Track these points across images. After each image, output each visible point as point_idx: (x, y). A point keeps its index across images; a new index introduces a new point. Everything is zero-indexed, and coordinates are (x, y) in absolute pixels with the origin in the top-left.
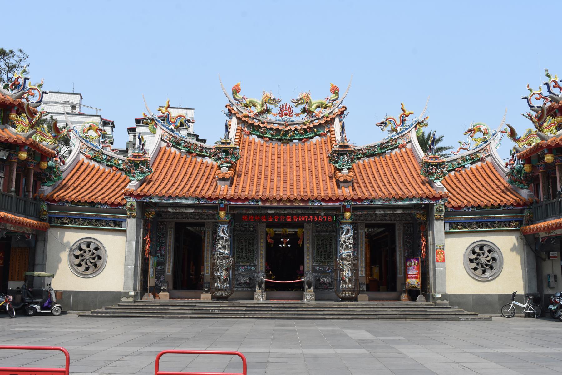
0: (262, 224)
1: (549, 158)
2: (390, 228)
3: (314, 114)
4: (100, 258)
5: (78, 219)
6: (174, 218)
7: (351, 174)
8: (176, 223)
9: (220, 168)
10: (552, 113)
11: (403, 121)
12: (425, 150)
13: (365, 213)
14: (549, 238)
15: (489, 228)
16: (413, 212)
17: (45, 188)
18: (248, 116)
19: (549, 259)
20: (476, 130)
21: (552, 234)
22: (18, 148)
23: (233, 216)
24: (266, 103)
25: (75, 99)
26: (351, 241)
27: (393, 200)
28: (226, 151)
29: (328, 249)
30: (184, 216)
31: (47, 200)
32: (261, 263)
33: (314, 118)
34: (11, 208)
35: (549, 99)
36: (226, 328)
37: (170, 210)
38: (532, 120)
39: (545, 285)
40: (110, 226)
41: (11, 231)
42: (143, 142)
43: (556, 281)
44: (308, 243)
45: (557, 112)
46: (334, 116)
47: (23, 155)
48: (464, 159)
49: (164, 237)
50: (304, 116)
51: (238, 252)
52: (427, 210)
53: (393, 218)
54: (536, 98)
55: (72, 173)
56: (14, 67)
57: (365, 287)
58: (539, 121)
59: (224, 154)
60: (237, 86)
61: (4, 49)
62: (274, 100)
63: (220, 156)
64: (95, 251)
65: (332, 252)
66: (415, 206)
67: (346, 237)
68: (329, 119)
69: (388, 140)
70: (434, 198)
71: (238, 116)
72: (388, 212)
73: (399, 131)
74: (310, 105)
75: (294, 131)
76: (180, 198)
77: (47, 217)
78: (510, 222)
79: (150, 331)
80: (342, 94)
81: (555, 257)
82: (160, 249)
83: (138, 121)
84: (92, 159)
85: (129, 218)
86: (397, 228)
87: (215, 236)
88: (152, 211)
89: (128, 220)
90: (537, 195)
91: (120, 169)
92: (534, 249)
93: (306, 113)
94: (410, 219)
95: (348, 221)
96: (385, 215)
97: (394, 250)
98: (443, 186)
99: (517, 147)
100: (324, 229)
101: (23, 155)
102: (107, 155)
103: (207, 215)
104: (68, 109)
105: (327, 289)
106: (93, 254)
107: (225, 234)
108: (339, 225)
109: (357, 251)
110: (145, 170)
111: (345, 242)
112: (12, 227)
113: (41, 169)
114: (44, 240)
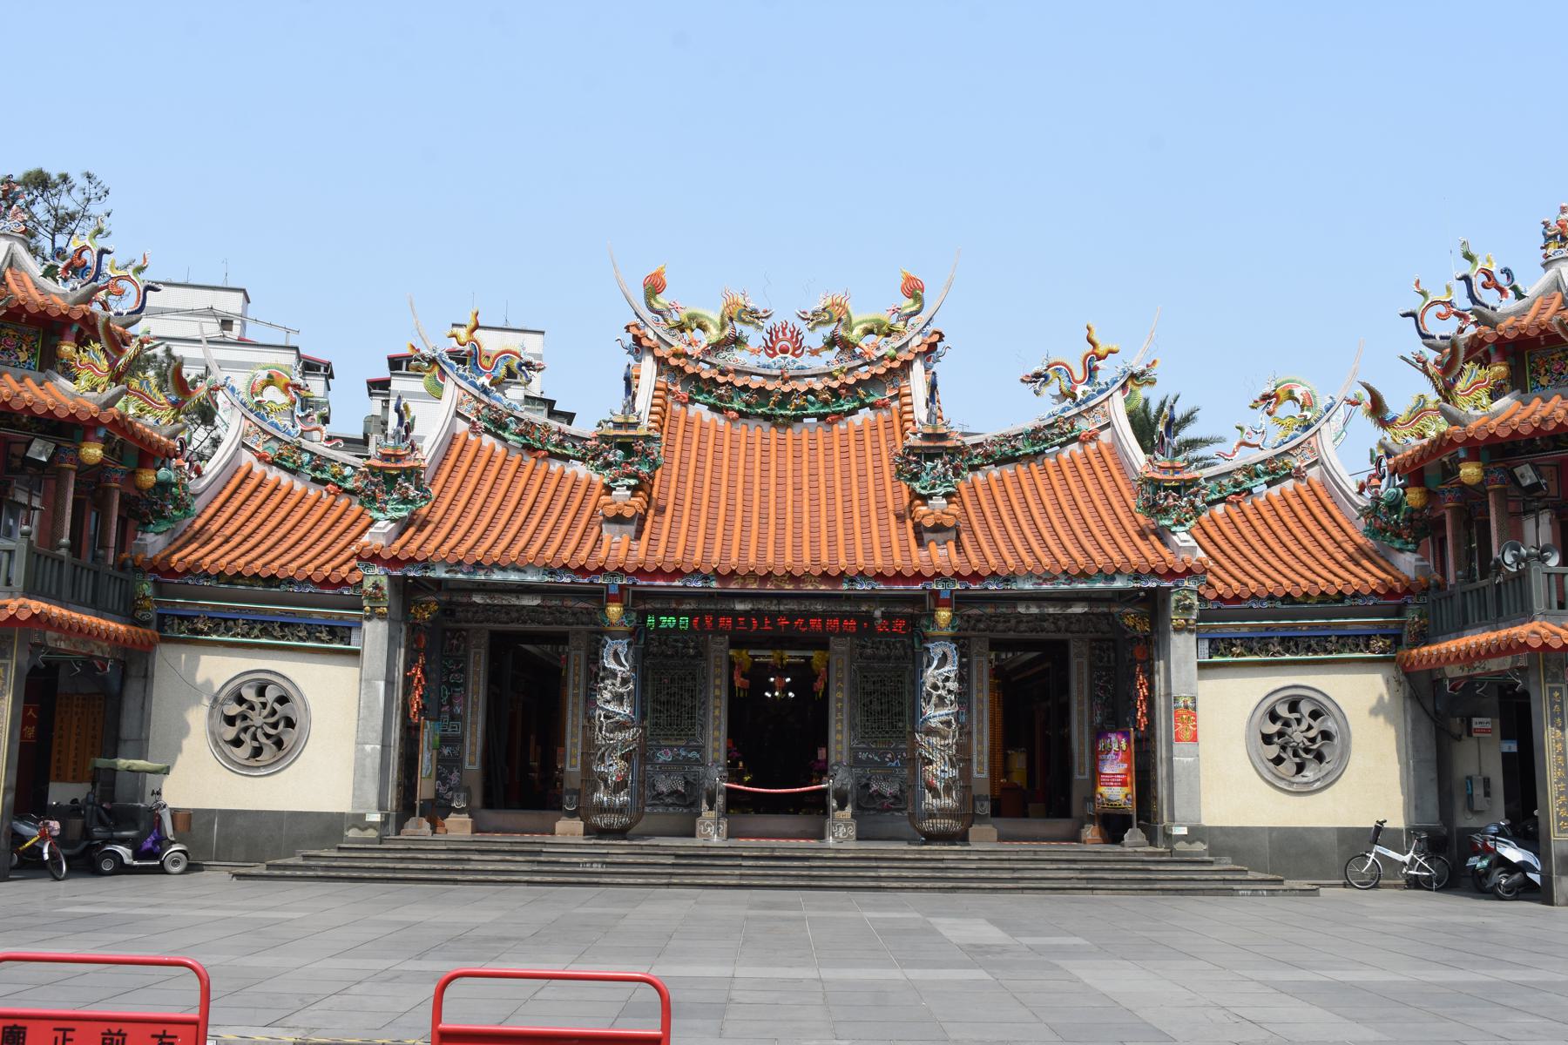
0: (719, 639)
1: (1470, 472)
2: (1056, 652)
3: (858, 350)
4: (290, 723)
5: (235, 620)
6: (488, 621)
7: (954, 509)
8: (494, 635)
9: (609, 490)
10: (1479, 354)
11: (1091, 372)
14: (1471, 682)
15: (1315, 652)
16: (1115, 610)
17: (150, 538)
18: (686, 355)
19: (1470, 734)
20: (1282, 395)
21: (1479, 671)
24: (731, 319)
25: (230, 304)
28: (627, 447)
29: (891, 707)
30: (514, 615)
32: (715, 740)
34: (59, 591)
37: (477, 599)
38: (1426, 371)
39: (1460, 803)
40: (319, 640)
41: (57, 651)
42: (407, 420)
44: (839, 689)
45: (1492, 351)
46: (910, 357)
48: (1251, 472)
49: (461, 671)
51: (654, 710)
53: (1062, 624)
54: (1439, 316)
56: (72, 217)
59: (620, 452)
60: (658, 275)
61: (46, 170)
62: (753, 312)
63: (611, 458)
64: (277, 706)
65: (901, 714)
66: (1121, 593)
68: (896, 364)
69: (1051, 420)
70: (1171, 574)
71: (658, 353)
72: (1051, 610)
73: (1080, 396)
74: (849, 326)
75: (806, 393)
76: (504, 569)
78: (1369, 637)
81: (1487, 731)
82: (450, 703)
83: (395, 363)
84: (273, 463)
85: (369, 618)
86: (1073, 651)
87: (595, 669)
88: (428, 603)
91: (346, 491)
93: (837, 349)
95: (945, 633)
97: (1065, 710)
98: (1193, 543)
99: (1389, 441)
101: (93, 452)
103: (574, 614)
104: (213, 329)
105: (888, 809)
106: (274, 712)
107: (621, 665)
108: (921, 643)
109: (969, 711)
110: (412, 493)
111: (935, 687)
113: (140, 489)
114: (146, 676)
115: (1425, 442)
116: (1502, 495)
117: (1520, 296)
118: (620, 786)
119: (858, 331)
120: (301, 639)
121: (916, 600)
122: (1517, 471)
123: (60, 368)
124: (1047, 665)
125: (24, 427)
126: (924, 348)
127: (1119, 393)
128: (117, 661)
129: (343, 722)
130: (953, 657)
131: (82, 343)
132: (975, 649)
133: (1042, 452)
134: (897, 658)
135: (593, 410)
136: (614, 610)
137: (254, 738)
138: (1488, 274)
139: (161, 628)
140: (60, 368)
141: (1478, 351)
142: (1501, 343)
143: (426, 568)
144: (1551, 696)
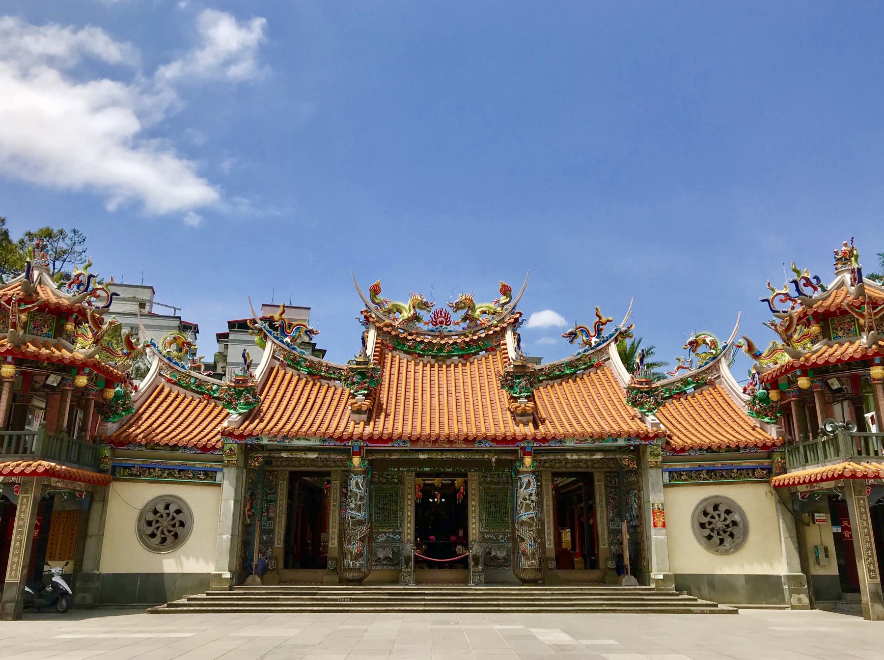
0: (410, 474)
1: (803, 382)
2: (587, 478)
3: (479, 322)
4: (182, 524)
5: (154, 469)
6: (288, 466)
7: (531, 404)
8: (291, 473)
9: (354, 396)
10: (804, 320)
11: (599, 332)
12: (630, 369)
13: (552, 457)
14: (812, 494)
15: (726, 478)
16: (618, 456)
17: (109, 425)
18: (391, 325)
19: (814, 523)
20: (700, 342)
21: (816, 488)
22: (75, 371)
23: (371, 462)
24: (414, 307)
25: (145, 295)
26: (534, 498)
27: (590, 440)
28: (363, 374)
29: (500, 507)
30: (302, 462)
31: (112, 442)
32: (409, 529)
33: (479, 328)
34: (60, 455)
35: (799, 301)
36: (365, 627)
37: (284, 455)
38: (776, 331)
39: (812, 561)
40: (199, 478)
41: (56, 488)
42: (248, 361)
43: (827, 556)
44: (473, 500)
45: (811, 319)
46: (505, 325)
47: (82, 381)
48: (685, 382)
49: (273, 493)
50: (464, 325)
51: (376, 513)
52: (637, 452)
53: (589, 464)
54: (781, 300)
55: (147, 403)
56: (65, 252)
57: (554, 563)
58: (787, 335)
59: (359, 377)
60: (377, 285)
61: (51, 227)
62: (426, 304)
63: (355, 380)
64: (175, 515)
65: (506, 513)
66: (620, 448)
67: (527, 489)
68: (498, 329)
69: (579, 356)
70: (647, 437)
71: (377, 325)
72: (584, 457)
73: (593, 344)
74: (473, 309)
75: (452, 344)
76: (299, 439)
77: (109, 467)
78: (754, 470)
79: (256, 635)
80: (516, 295)
81: (824, 521)
82: (267, 511)
83: (232, 325)
84: (175, 383)
85: (227, 466)
86: (596, 478)
87: (345, 491)
88: (258, 458)
89: (225, 470)
90: (790, 430)
91: (214, 398)
92: (791, 509)
93: (468, 322)
94: (613, 466)
95: (529, 470)
96: (579, 461)
97: (592, 509)
98: (658, 421)
99: (758, 365)
100: (495, 480)
101: (82, 381)
102: (196, 378)
103: (334, 462)
104: (134, 307)
105: (501, 566)
106: (174, 518)
107: (360, 489)
108: (516, 475)
109: (542, 511)
110: (251, 400)
111: (525, 499)
112: (58, 482)
113: (105, 399)
114: (104, 500)
115: (778, 366)
116: (822, 394)
117: (824, 290)
118: (359, 555)
119: (478, 312)
120: (189, 478)
121: (515, 452)
122: (829, 381)
123: (65, 336)
124: (581, 484)
125: (45, 368)
126: (512, 320)
127: (613, 344)
128: (88, 492)
129: (213, 512)
130: (534, 484)
131: (78, 324)
132: (544, 478)
133: (575, 373)
134: (503, 483)
135: (339, 357)
136: (356, 460)
137: (163, 533)
138: (807, 279)
139: (113, 473)
140: (65, 336)
141: (805, 320)
142: (816, 315)
143: (258, 439)
144: (859, 503)
